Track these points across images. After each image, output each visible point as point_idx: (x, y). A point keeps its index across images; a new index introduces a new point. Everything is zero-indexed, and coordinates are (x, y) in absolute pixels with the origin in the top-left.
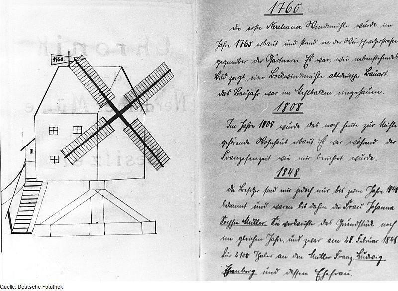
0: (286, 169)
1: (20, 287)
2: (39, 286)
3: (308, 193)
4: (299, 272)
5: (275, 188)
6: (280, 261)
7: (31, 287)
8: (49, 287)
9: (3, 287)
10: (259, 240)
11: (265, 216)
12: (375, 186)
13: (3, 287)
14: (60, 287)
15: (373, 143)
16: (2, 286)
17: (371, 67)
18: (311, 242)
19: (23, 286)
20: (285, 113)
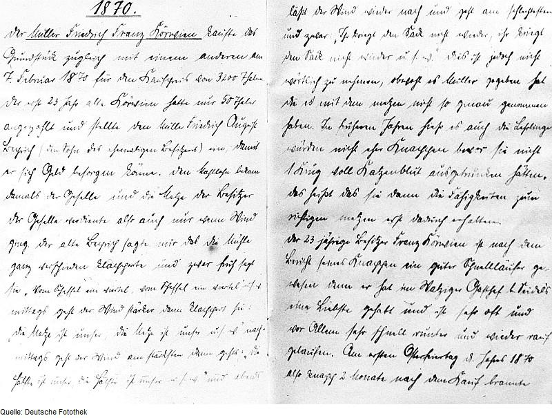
2: (55, 412)
3: (505, 60)
4: (101, 103)
5: (255, 215)
7: (42, 413)
8: (68, 412)
9: (5, 413)
11: (156, 300)
13: (5, 413)
14: (83, 412)
16: (3, 412)
17: (423, 159)
18: (198, 266)
20: (106, 16)
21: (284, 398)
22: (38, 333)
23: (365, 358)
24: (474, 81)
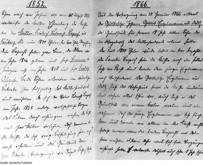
0: (87, 14)
1: (10, 163)
2: (20, 163)
6: (152, 45)
8: (25, 163)
9: (2, 163)
10: (184, 79)
12: (192, 150)
14: (31, 163)
15: (196, 14)
16: (1, 163)
19: (12, 163)
21: (99, 158)
22: (13, 137)
23: (191, 80)
24: (124, 131)
